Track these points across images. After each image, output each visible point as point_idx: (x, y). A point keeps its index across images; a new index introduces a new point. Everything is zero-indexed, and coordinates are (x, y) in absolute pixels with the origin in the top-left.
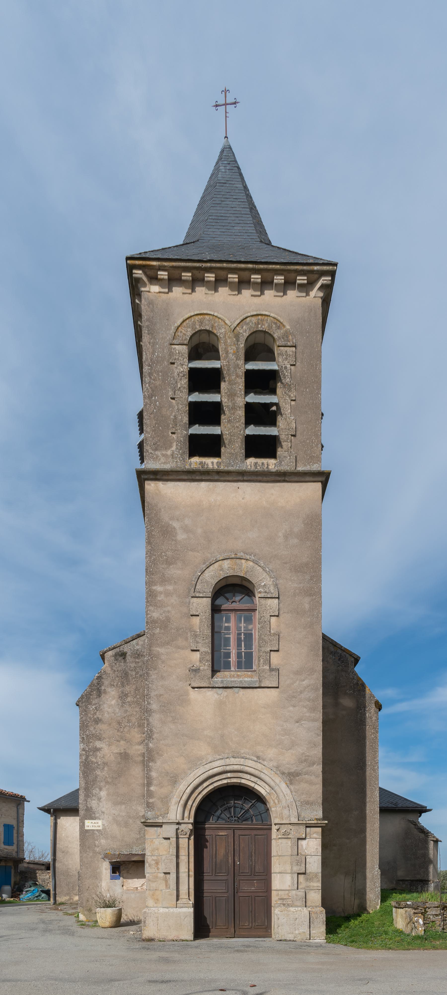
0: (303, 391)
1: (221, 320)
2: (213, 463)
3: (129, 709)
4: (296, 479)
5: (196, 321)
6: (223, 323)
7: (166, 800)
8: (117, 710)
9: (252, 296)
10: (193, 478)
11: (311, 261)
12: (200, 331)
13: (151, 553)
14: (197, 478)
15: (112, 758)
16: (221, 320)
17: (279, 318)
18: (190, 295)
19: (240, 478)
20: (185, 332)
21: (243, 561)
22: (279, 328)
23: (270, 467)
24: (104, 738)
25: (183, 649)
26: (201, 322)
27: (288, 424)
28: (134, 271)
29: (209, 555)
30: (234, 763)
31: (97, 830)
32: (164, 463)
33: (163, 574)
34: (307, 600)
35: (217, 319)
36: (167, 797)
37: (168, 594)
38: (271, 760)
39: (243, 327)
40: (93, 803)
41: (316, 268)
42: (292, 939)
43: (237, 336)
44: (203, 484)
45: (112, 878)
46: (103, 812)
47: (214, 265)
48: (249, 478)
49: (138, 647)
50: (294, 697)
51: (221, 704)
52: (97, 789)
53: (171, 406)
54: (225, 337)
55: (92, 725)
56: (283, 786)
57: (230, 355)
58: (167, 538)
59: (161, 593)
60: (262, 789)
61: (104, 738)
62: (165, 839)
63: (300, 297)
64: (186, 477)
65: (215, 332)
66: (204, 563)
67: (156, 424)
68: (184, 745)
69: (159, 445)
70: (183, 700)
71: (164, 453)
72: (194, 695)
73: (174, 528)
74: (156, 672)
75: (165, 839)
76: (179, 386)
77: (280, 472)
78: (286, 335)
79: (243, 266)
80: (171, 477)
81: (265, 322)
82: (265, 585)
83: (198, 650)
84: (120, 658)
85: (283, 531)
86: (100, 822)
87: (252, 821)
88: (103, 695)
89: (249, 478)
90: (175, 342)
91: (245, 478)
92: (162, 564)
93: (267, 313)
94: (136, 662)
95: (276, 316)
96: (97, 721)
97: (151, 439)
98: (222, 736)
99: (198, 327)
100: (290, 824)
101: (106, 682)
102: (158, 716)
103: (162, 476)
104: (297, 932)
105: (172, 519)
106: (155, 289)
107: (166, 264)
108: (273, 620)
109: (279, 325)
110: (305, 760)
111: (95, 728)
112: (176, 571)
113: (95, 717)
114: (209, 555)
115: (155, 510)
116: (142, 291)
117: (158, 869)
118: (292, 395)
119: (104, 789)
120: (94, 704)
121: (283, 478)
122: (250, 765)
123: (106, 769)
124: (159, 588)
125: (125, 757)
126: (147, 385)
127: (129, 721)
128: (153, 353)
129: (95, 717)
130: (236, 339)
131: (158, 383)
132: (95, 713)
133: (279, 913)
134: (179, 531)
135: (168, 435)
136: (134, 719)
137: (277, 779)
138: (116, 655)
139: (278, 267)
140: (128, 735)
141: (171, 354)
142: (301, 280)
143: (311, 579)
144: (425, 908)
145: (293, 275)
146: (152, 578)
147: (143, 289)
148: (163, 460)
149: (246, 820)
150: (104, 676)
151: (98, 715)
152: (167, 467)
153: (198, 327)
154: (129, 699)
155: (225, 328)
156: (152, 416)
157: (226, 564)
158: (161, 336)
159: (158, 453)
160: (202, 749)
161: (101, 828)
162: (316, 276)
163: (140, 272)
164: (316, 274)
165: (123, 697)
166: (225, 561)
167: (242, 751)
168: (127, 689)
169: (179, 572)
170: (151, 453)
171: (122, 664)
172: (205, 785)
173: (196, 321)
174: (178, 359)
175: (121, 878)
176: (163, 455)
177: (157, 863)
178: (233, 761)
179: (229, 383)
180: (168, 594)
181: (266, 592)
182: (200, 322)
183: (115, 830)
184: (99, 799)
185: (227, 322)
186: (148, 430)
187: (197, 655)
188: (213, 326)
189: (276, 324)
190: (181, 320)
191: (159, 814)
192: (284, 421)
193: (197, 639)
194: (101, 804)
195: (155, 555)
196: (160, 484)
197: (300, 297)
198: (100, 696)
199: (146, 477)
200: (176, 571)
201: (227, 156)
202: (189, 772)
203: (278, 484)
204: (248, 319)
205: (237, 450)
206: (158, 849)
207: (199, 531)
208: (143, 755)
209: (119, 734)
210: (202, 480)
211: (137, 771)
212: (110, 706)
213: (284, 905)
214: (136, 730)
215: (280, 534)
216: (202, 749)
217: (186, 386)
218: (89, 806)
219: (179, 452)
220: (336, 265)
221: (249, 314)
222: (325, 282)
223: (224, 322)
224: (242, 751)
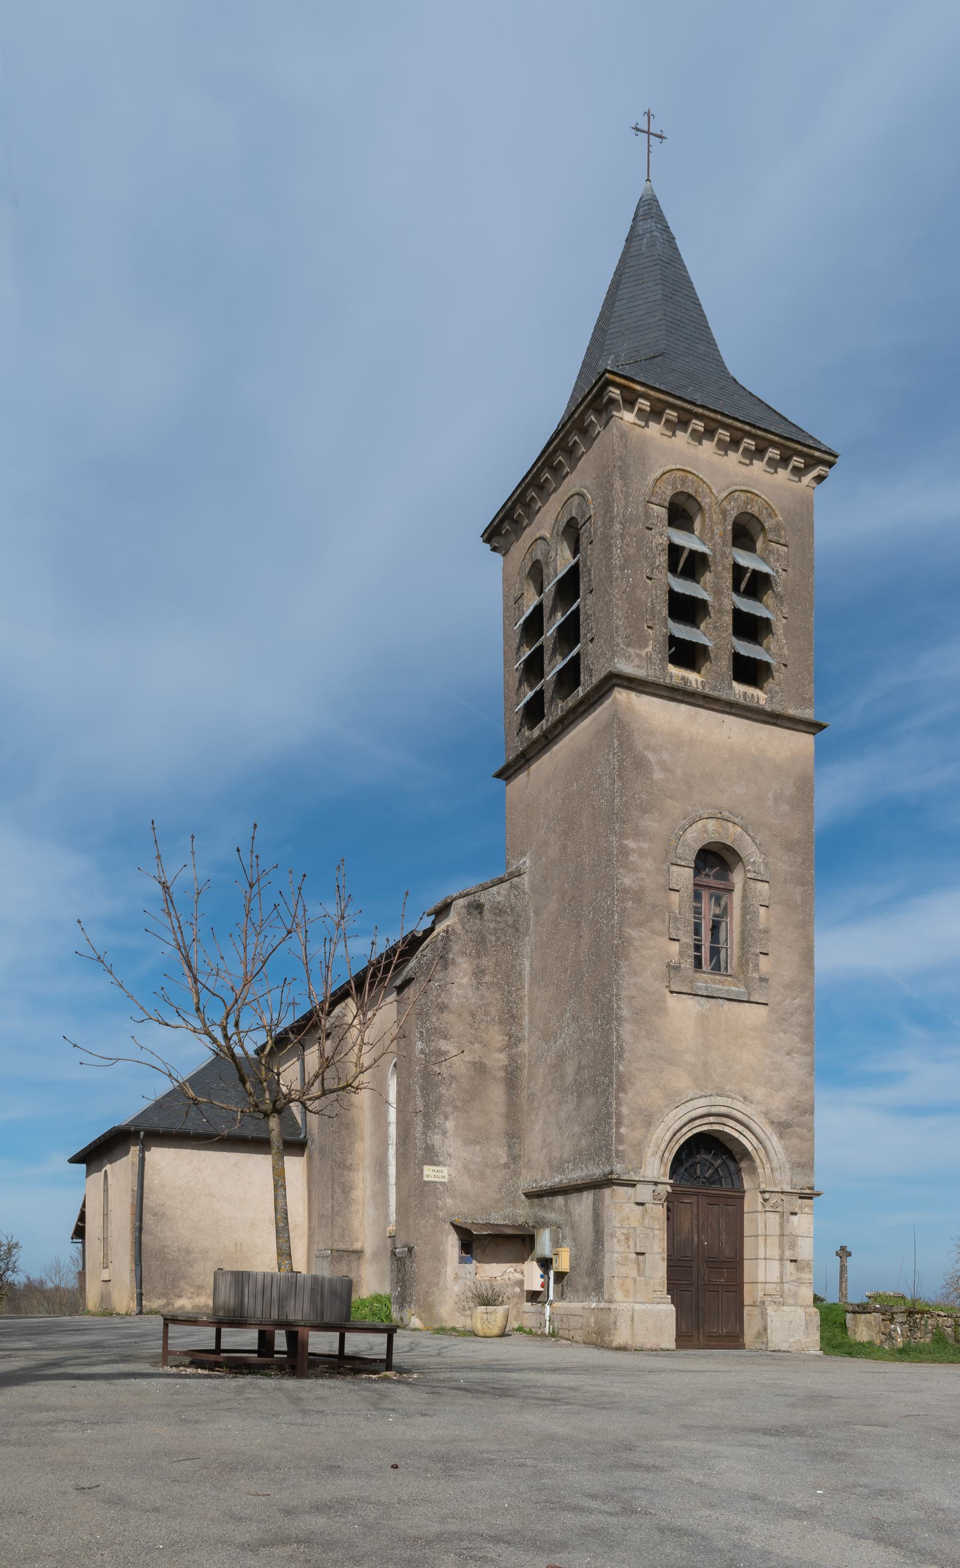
2: (697, 681)
3: (487, 994)
4: (788, 725)
6: (708, 490)
7: (639, 1148)
8: (471, 993)
10: (674, 696)
11: (811, 443)
14: (679, 697)
15: (463, 1069)
17: (771, 503)
19: (728, 709)
21: (730, 825)
22: (770, 515)
24: (452, 1037)
25: (660, 935)
26: (683, 481)
27: (780, 649)
28: (611, 389)
30: (720, 1104)
31: (441, 1183)
32: (638, 667)
34: (798, 890)
35: (701, 483)
36: (639, 1144)
37: (642, 854)
38: (759, 1103)
40: (436, 1139)
41: (817, 454)
42: (786, 1349)
43: (724, 512)
44: (683, 707)
45: (462, 1261)
46: (450, 1155)
47: (707, 413)
49: (499, 898)
50: (784, 1020)
51: (703, 1019)
52: (442, 1117)
54: (710, 509)
55: (434, 1013)
56: (775, 1139)
57: (717, 537)
59: (633, 850)
60: (748, 1142)
61: (452, 1037)
62: (637, 1204)
64: (666, 694)
65: (699, 500)
68: (661, 1072)
70: (661, 1010)
71: (638, 651)
72: (672, 1002)
73: (650, 761)
74: (627, 963)
75: (637, 1204)
78: (778, 528)
79: (739, 425)
80: (648, 690)
81: (754, 503)
82: (754, 862)
83: (678, 940)
84: (475, 912)
86: (445, 1171)
87: (721, 1184)
88: (450, 968)
90: (654, 499)
91: (733, 711)
93: (757, 492)
94: (497, 922)
95: (767, 499)
96: (442, 1008)
98: (705, 1063)
100: (782, 1193)
101: (456, 947)
102: (630, 1027)
104: (792, 1340)
105: (647, 747)
107: (652, 393)
108: (762, 910)
109: (772, 514)
110: (797, 1107)
111: (438, 1019)
113: (439, 1000)
116: (613, 416)
117: (628, 1247)
119: (451, 1117)
120: (438, 981)
122: (739, 1108)
123: (454, 1085)
124: (631, 844)
125: (480, 1068)
127: (487, 1013)
129: (439, 1000)
132: (439, 995)
133: (773, 1313)
134: (656, 768)
136: (493, 1011)
137: (769, 1130)
138: (469, 906)
139: (777, 439)
140: (484, 1035)
141: (647, 514)
142: (797, 461)
143: (803, 863)
144: (892, 1314)
145: (789, 453)
147: (615, 413)
148: (636, 662)
149: (714, 1183)
150: (452, 937)
151: (443, 998)
154: (487, 978)
157: (711, 824)
159: (631, 650)
160: (682, 1081)
161: (445, 1180)
162: (813, 462)
163: (618, 392)
165: (479, 973)
167: (727, 1088)
168: (485, 962)
169: (655, 825)
171: (478, 922)
172: (684, 1130)
175: (474, 1262)
177: (627, 1239)
178: (720, 1100)
180: (642, 854)
181: (755, 872)
183: (466, 1184)
184: (444, 1133)
185: (714, 490)
187: (675, 947)
188: (696, 491)
189: (766, 509)
190: (660, 472)
191: (630, 1167)
193: (678, 925)
194: (446, 1141)
196: (633, 695)
198: (446, 969)
199: (619, 682)
201: (649, 210)
202: (666, 1111)
203: (767, 726)
204: (736, 493)
206: (628, 1219)
207: (679, 772)
208: (506, 1068)
209: (472, 1031)
211: (497, 1093)
212: (461, 986)
213: (775, 1302)
214: (496, 1028)
215: (770, 796)
216: (682, 1081)
218: (429, 1142)
220: (836, 457)
223: (710, 489)
224: (727, 1088)
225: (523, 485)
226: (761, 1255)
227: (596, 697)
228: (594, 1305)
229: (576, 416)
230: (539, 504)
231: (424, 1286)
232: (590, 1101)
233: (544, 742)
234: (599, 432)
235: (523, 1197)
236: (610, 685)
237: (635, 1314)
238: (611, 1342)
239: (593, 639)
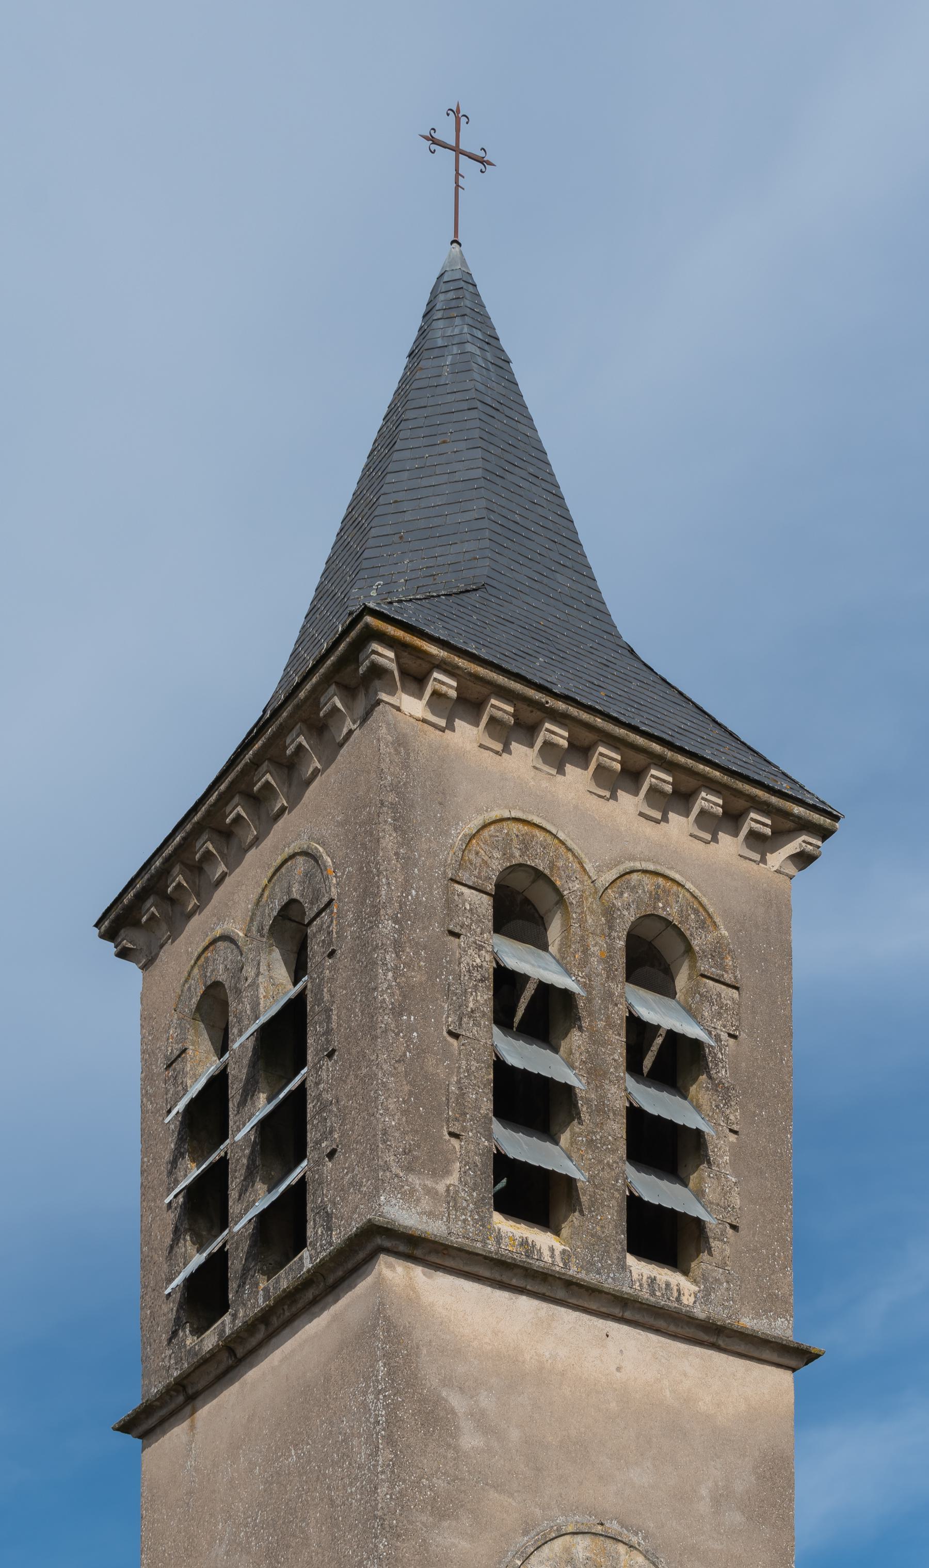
0: (754, 1115)
1: (574, 855)
4: (742, 1348)
5: (514, 837)
6: (576, 866)
9: (641, 814)
10: (505, 1279)
11: (785, 787)
12: (520, 865)
13: (393, 1472)
14: (514, 1282)
16: (574, 855)
18: (498, 757)
19: (617, 1311)
20: (486, 858)
22: (702, 925)
23: (685, 1300)
26: (526, 845)
29: (538, 1512)
33: (424, 1540)
35: (562, 850)
39: (621, 894)
41: (797, 810)
43: (609, 912)
47: (574, 711)
48: (638, 1317)
53: (446, 1052)
54: (580, 904)
57: (594, 960)
58: (436, 1436)
63: (746, 858)
64: (487, 1273)
66: (525, 1533)
67: (410, 1093)
69: (416, 1158)
71: (429, 1183)
76: (471, 1005)
77: (714, 1324)
78: (718, 951)
80: (449, 1263)
85: (710, 1484)
89: (638, 1317)
90: (464, 876)
91: (628, 1315)
92: (422, 1511)
93: (677, 877)
95: (698, 893)
97: (397, 1134)
99: (517, 854)
103: (430, 1252)
105: (447, 1382)
106: (413, 706)
107: (461, 662)
109: (707, 922)
112: (456, 1541)
114: (538, 1512)
115: (406, 1347)
118: (732, 1117)
121: (712, 1339)
126: (390, 974)
128: (406, 886)
130: (608, 921)
131: (417, 978)
134: (466, 1425)
135: (441, 1137)
141: (450, 906)
146: (396, 1549)
147: (384, 696)
148: (426, 1203)
152: (435, 1228)
153: (517, 854)
155: (582, 882)
156: (401, 1068)
158: (425, 847)
163: (391, 655)
164: (793, 821)
166: (579, 1538)
169: (464, 1544)
170: (397, 1176)
173: (514, 837)
174: (469, 926)
176: (429, 1191)
179: (590, 1038)
182: (523, 842)
186: (392, 1107)
188: (552, 866)
189: (696, 912)
190: (477, 822)
192: (715, 1182)
195: (404, 1481)
197: (746, 858)
199: (387, 1244)
200: (456, 1541)
201: (455, 301)
203: (698, 1350)
204: (635, 876)
205: (610, 1230)
207: (515, 1435)
210: (521, 1291)
215: (704, 1492)
217: (488, 1010)
219: (471, 1195)
220: (836, 818)
221: (638, 865)
222: (810, 848)
223: (581, 863)
227: (340, 1273)
229: (302, 694)
234: (351, 732)
236: (370, 1247)
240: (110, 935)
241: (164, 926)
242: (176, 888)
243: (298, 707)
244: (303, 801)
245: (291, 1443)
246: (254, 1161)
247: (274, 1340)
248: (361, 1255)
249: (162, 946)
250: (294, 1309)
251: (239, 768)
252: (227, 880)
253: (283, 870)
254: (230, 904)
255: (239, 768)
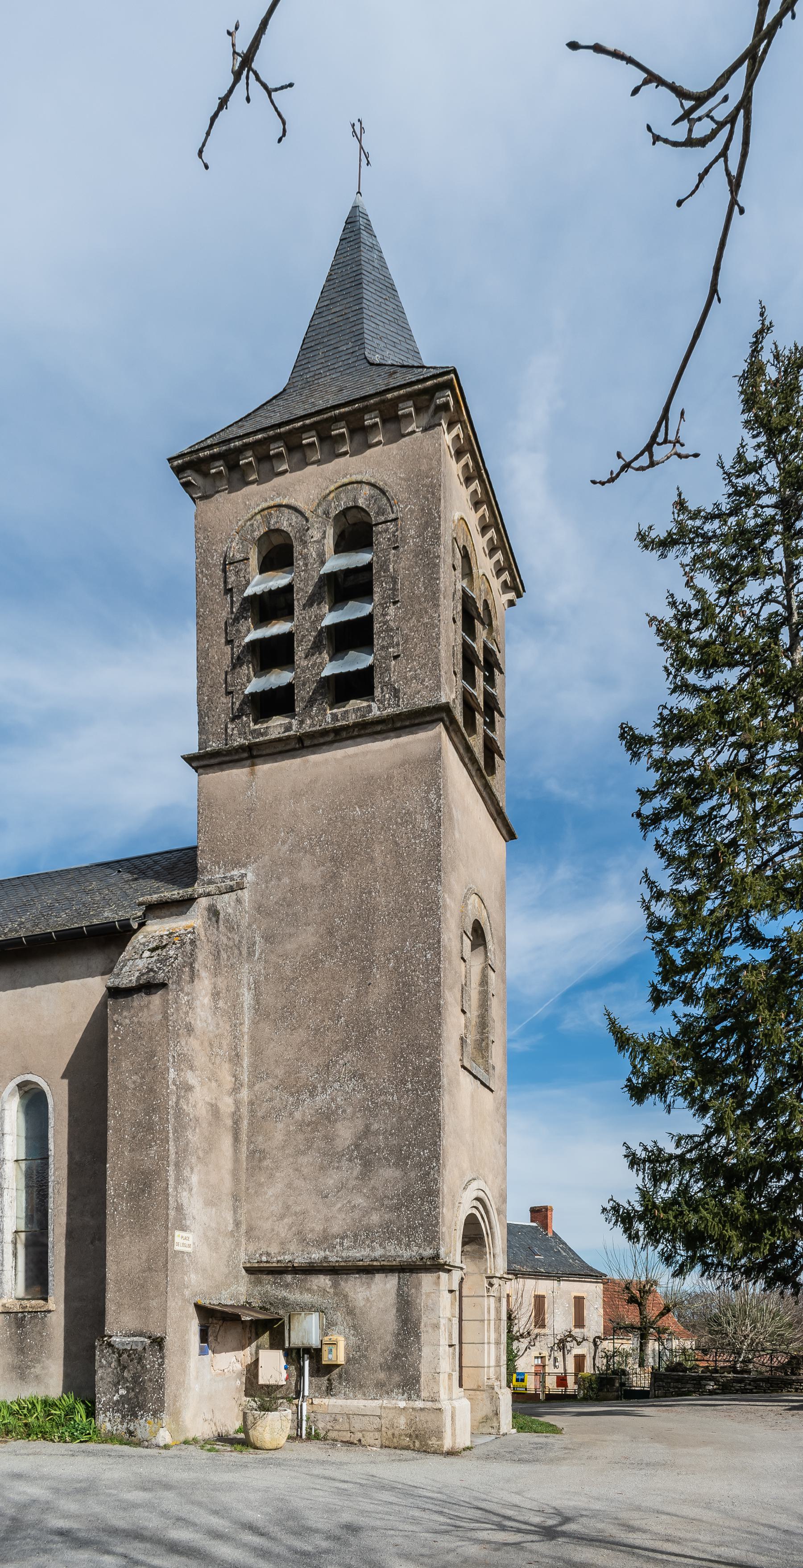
8: (210, 1018)
123: (197, 1130)
161: (189, 1250)
225: (271, 433)
226: (486, 1341)
227: (407, 723)
228: (402, 1404)
229: (389, 396)
230: (285, 467)
231: (173, 1387)
232: (387, 1175)
233: (293, 744)
234: (414, 432)
235: (243, 1271)
236: (436, 716)
237: (457, 1412)
238: (442, 1446)
239: (398, 656)
240: (178, 471)
241: (225, 482)
242: (247, 464)
243: (383, 402)
244: (364, 454)
245: (356, 804)
246: (321, 641)
247: (336, 745)
248: (428, 719)
249: (218, 492)
250: (362, 732)
251: (325, 416)
252: (288, 475)
253: (349, 487)
254: (291, 489)
255: (325, 416)
